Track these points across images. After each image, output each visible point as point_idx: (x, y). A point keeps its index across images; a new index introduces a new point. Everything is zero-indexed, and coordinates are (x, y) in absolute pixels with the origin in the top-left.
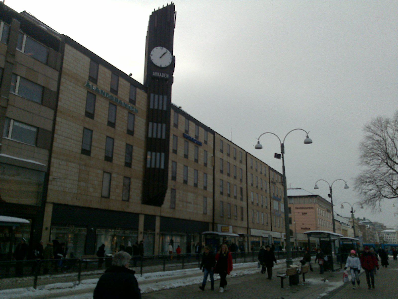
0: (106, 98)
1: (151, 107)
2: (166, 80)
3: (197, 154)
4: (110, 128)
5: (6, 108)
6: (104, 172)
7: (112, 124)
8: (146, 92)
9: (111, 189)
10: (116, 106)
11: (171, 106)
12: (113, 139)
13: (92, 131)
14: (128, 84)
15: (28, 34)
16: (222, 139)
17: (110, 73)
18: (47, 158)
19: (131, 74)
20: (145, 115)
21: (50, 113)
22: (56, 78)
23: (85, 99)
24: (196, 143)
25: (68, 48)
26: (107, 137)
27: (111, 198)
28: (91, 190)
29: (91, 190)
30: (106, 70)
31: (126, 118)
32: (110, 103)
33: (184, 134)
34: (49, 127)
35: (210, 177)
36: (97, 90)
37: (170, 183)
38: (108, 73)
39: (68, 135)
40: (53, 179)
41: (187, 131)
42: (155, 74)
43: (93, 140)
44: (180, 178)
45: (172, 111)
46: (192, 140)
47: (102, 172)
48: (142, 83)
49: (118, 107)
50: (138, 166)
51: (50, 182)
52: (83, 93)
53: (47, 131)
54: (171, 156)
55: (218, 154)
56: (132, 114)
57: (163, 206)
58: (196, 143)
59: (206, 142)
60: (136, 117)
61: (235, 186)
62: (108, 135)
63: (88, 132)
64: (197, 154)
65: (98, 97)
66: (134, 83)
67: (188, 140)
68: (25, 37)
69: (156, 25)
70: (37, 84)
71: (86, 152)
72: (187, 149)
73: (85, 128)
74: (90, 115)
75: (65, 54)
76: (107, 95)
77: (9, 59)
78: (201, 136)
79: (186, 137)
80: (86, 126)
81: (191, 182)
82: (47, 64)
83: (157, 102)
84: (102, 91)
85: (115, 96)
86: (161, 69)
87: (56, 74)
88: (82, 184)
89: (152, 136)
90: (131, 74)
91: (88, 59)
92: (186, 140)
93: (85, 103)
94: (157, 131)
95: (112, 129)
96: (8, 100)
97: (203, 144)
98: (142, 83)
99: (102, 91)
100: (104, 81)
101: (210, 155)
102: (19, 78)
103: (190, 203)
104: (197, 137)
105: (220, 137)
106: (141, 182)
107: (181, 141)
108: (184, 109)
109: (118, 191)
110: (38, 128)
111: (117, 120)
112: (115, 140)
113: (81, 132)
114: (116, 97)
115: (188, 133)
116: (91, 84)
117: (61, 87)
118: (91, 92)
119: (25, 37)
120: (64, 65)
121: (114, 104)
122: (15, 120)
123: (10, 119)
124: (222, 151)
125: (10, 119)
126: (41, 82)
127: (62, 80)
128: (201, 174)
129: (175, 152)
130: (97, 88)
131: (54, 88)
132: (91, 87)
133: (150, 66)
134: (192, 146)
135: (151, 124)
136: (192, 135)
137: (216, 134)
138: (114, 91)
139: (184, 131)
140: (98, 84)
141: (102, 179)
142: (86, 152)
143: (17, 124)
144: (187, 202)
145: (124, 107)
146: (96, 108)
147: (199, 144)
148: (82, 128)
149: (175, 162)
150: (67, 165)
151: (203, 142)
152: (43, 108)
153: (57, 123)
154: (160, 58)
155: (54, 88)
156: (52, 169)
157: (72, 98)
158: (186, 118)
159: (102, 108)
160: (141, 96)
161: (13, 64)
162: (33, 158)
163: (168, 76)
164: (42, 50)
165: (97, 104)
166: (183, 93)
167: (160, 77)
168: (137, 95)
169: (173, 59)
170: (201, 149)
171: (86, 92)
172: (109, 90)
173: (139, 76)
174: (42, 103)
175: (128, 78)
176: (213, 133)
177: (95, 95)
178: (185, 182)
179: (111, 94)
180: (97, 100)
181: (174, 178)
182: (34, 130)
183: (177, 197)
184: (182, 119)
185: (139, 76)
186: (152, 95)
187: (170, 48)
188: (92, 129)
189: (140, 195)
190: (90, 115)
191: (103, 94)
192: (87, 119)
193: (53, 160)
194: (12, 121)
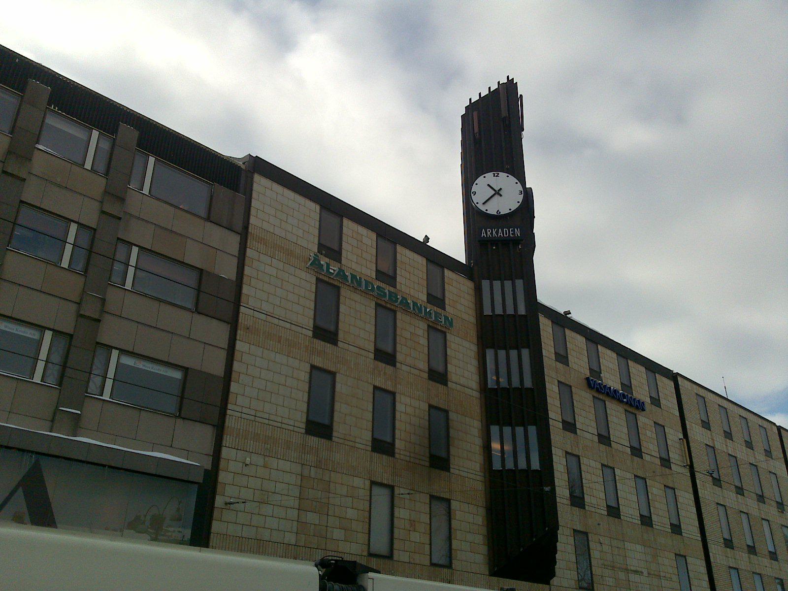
0: (366, 293)
1: (487, 311)
2: (516, 241)
3: (635, 430)
4: (381, 365)
5: (99, 321)
6: (373, 483)
7: (386, 357)
8: (471, 278)
9: (396, 531)
10: (395, 312)
11: (536, 308)
12: (393, 394)
13: (333, 374)
14: (421, 261)
15: (157, 154)
16: (702, 392)
17: (374, 236)
18: (209, 448)
19: (427, 239)
20: (473, 333)
21: (218, 332)
22: (235, 249)
23: (313, 296)
24: (627, 403)
25: (260, 183)
26: (376, 388)
27: (396, 557)
28: (338, 534)
29: (338, 534)
30: (362, 230)
31: (424, 342)
32: (377, 305)
33: (587, 379)
34: (218, 370)
35: (686, 498)
36: (341, 274)
37: (567, 517)
38: (369, 237)
39: (269, 385)
40: (226, 504)
41: (596, 372)
42: (487, 233)
43: (337, 398)
44: (596, 496)
45: (545, 325)
46: (613, 395)
47: (368, 483)
48: (463, 260)
49: (399, 315)
50: (467, 463)
51: (216, 514)
52: (303, 285)
53: (209, 376)
54: (559, 438)
55: (696, 432)
56: (438, 331)
57: (555, 581)
58: (627, 403)
59: (656, 402)
60: (448, 336)
61: (765, 523)
62: (377, 384)
63: (322, 380)
64: (635, 430)
65: (345, 292)
66: (438, 260)
67: (601, 397)
68: (152, 160)
69: (476, 130)
70: (182, 263)
71: (319, 428)
72: (603, 420)
73: (313, 367)
74: (326, 333)
75: (254, 195)
76: (366, 287)
77: (108, 208)
78: (633, 385)
79: (594, 384)
80: (318, 362)
81: (630, 510)
82: (208, 219)
83: (501, 297)
84: (415, 304)
85: (387, 289)
86: (498, 219)
87: (232, 242)
88: (312, 518)
89: (498, 382)
90: (427, 239)
91: (313, 208)
92: (596, 395)
93: (312, 306)
94: (509, 370)
95: (389, 369)
96: (103, 301)
97: (648, 406)
98: (463, 260)
99: (415, 304)
100: (359, 255)
101: (674, 435)
102: (135, 250)
103: (636, 572)
104: (627, 386)
105: (695, 386)
106: (482, 511)
107: (584, 399)
108: (575, 316)
109: (415, 537)
110: (186, 370)
111: (398, 347)
112: (398, 397)
113: (304, 376)
114: (392, 289)
115: (600, 378)
116: (324, 261)
117: (247, 270)
118: (326, 279)
119: (152, 160)
120: (253, 220)
121: (388, 308)
122: (123, 351)
123: (110, 348)
124: (706, 425)
125: (110, 348)
126: (193, 257)
127: (249, 252)
128: (656, 490)
129: (570, 427)
130: (341, 270)
131: (228, 271)
132: (325, 268)
133: (474, 218)
134: (616, 413)
135: (490, 354)
136: (612, 381)
137: (679, 379)
138: (388, 277)
139: (588, 373)
140: (344, 261)
141: (367, 504)
142: (319, 428)
143: (128, 361)
144: (627, 570)
145: (416, 311)
146: (341, 317)
147: (640, 406)
148: (307, 368)
149: (573, 457)
150: (265, 466)
151: (648, 400)
152: (200, 320)
153: (237, 355)
154: (488, 185)
155: (228, 271)
156: (222, 477)
157: (278, 292)
158: (587, 339)
159: (357, 318)
160: (459, 291)
161: (120, 219)
162: (170, 447)
163: (518, 232)
164: (196, 190)
165: (342, 308)
166: (559, 275)
167: (503, 243)
168: (446, 286)
169: (528, 195)
170: (642, 419)
171: (314, 280)
172: (374, 276)
173: (451, 241)
174: (197, 310)
175: (422, 248)
176: (674, 377)
177: (338, 288)
178: (614, 512)
179: (377, 284)
180: (342, 299)
181: (578, 501)
182: (178, 375)
183: (595, 554)
184: (576, 342)
185: (451, 241)
186: (485, 284)
187: (517, 171)
188: (333, 369)
189: (484, 549)
190: (326, 333)
191: (356, 283)
192: (319, 344)
193: (225, 452)
194: (115, 353)
